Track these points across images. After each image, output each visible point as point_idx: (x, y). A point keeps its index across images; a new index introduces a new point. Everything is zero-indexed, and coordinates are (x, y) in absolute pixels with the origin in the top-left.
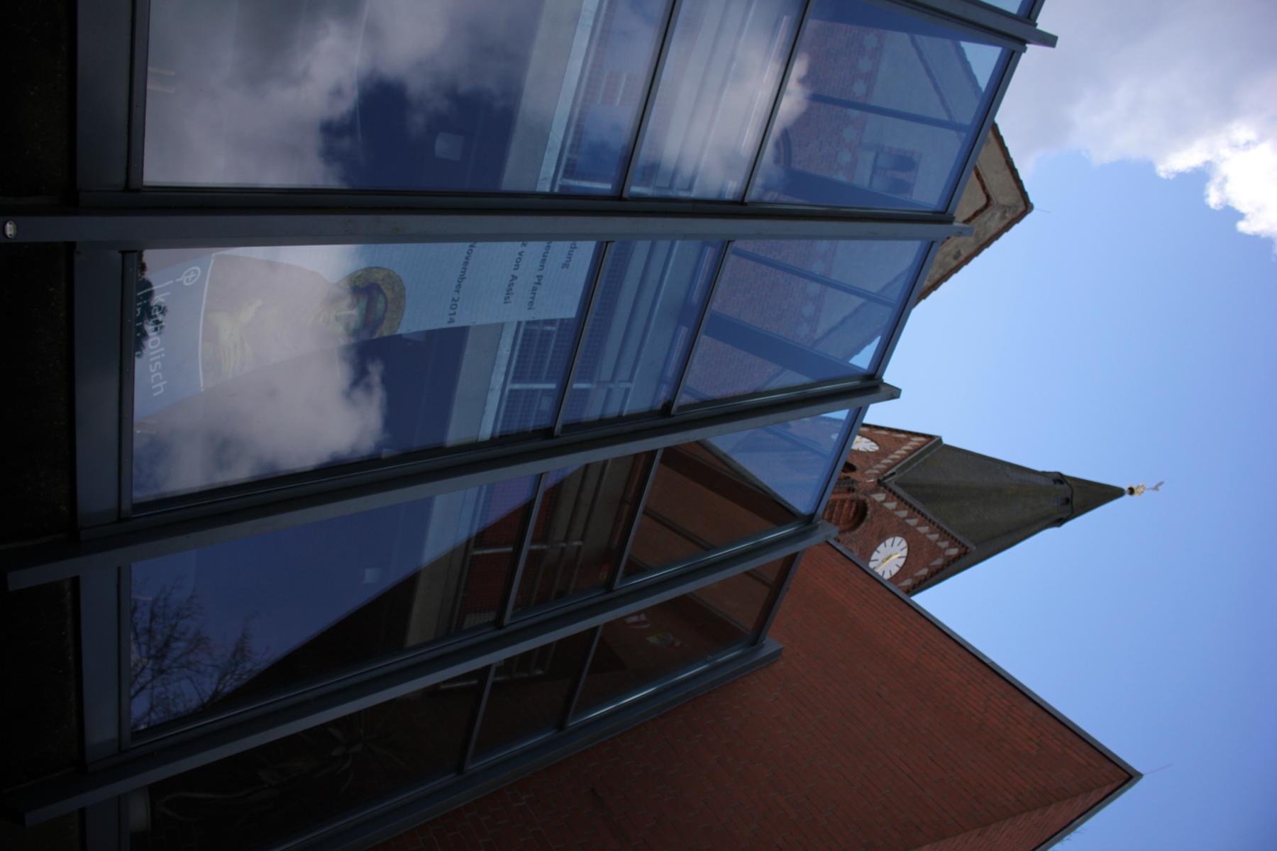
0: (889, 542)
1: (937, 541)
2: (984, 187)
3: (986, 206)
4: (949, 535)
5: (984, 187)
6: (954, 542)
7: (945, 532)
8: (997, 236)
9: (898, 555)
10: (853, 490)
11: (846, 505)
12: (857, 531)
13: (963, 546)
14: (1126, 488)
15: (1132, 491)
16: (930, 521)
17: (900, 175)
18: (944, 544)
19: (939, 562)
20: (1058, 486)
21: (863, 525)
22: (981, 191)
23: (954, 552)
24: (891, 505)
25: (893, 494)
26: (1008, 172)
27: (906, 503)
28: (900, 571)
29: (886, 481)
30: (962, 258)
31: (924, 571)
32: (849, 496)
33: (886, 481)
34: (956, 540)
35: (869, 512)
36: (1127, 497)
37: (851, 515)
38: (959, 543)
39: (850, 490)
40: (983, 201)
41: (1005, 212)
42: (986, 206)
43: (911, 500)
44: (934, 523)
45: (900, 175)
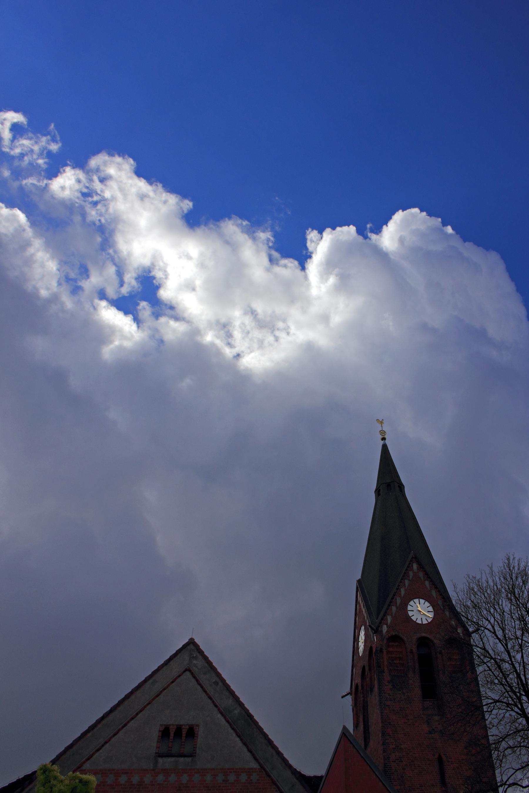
0: (410, 614)
1: (409, 580)
2: (180, 676)
3: (190, 671)
4: (405, 573)
5: (180, 676)
6: (410, 567)
7: (404, 576)
8: (206, 658)
9: (418, 605)
10: (381, 649)
11: (391, 649)
12: (405, 639)
13: (411, 561)
14: (382, 442)
15: (384, 439)
16: (397, 589)
17: (184, 733)
18: (411, 574)
19: (421, 574)
20: (381, 492)
21: (401, 635)
22: (182, 677)
23: (415, 566)
24: (389, 619)
25: (383, 620)
26: (172, 662)
27: (387, 609)
28: (427, 601)
29: (375, 628)
30: (218, 679)
31: (427, 583)
32: (385, 651)
33: (375, 628)
34: (408, 567)
35: (394, 634)
36: (387, 442)
37: (397, 644)
38: (410, 564)
39: (381, 651)
40: (188, 673)
41: (193, 657)
42: (190, 671)
43: (386, 606)
44: (399, 586)
45: (184, 733)
